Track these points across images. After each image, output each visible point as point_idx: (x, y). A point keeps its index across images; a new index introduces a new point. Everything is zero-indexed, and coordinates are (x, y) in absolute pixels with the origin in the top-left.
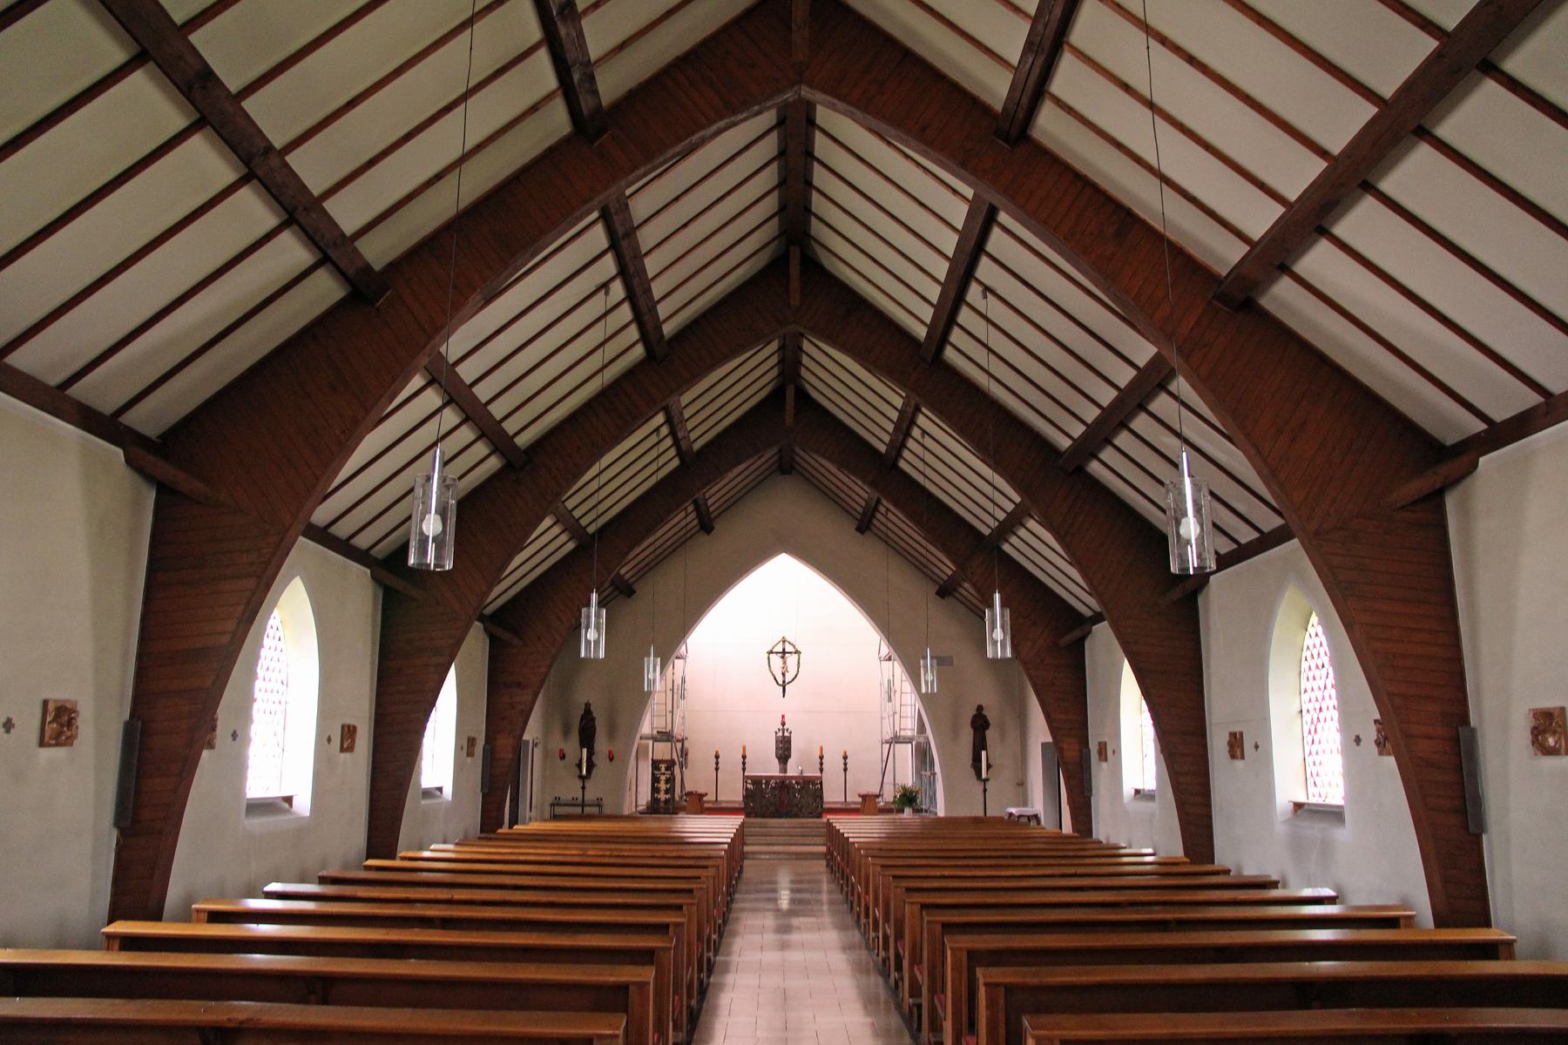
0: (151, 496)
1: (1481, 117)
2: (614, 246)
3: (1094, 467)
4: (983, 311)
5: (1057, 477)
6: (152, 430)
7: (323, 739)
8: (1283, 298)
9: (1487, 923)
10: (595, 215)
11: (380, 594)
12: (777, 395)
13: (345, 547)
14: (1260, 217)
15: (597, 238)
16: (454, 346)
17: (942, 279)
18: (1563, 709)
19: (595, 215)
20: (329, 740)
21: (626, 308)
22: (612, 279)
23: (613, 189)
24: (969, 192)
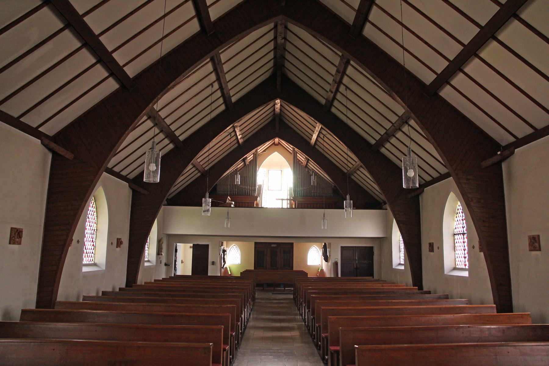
0: (50, 156)
1: (512, 33)
2: (215, 70)
3: (383, 150)
4: (345, 95)
5: (369, 153)
6: (51, 133)
7: (110, 244)
8: (446, 93)
9: (256, 243)
10: (209, 60)
11: (131, 192)
12: (273, 77)
13: (118, 175)
14: (441, 65)
15: (210, 67)
16: (157, 106)
17: (337, 65)
18: (539, 236)
19: (209, 60)
20: (438, 248)
21: (219, 92)
22: (214, 82)
23: (215, 50)
24: (340, 54)
